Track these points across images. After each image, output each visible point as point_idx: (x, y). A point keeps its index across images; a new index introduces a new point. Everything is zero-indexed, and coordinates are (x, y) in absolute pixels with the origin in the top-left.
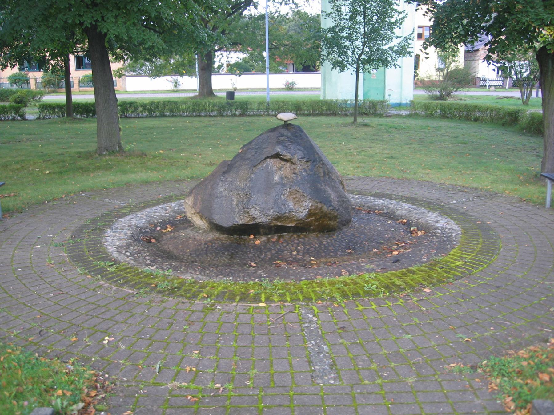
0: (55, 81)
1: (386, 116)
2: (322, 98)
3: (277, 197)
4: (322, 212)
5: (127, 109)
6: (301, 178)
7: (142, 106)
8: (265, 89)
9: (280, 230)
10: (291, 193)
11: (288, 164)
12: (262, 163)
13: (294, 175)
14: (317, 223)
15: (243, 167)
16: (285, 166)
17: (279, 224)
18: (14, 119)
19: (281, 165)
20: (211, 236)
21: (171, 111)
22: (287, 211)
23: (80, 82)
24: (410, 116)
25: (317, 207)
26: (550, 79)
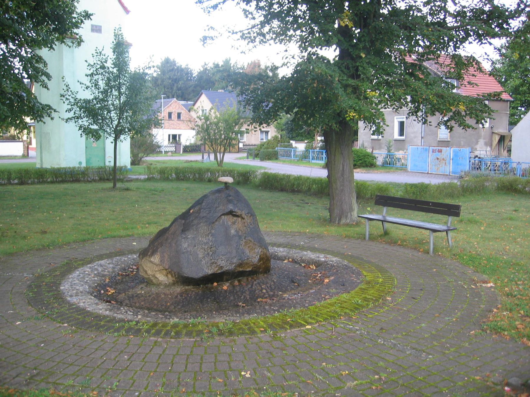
1: (127, 181)
2: (38, 166)
12: (218, 220)
15: (202, 224)
17: (241, 270)
20: (178, 289)
24: (149, 179)
26: (334, 146)
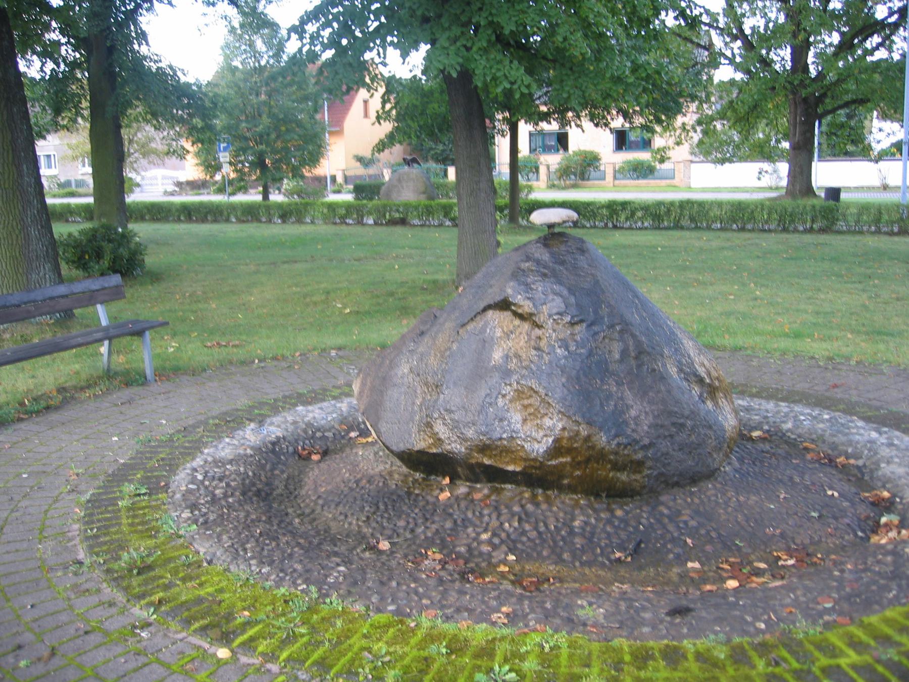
0: (576, 169)
3: (488, 400)
4: (593, 447)
5: (617, 215)
6: (550, 362)
7: (642, 209)
8: (899, 188)
9: (495, 475)
10: (520, 394)
11: (526, 326)
12: (478, 318)
13: (534, 352)
14: (578, 473)
16: (519, 330)
17: (487, 461)
18: (441, 225)
19: (511, 327)
21: (692, 219)
22: (505, 436)
23: (615, 171)
25: (578, 433)
